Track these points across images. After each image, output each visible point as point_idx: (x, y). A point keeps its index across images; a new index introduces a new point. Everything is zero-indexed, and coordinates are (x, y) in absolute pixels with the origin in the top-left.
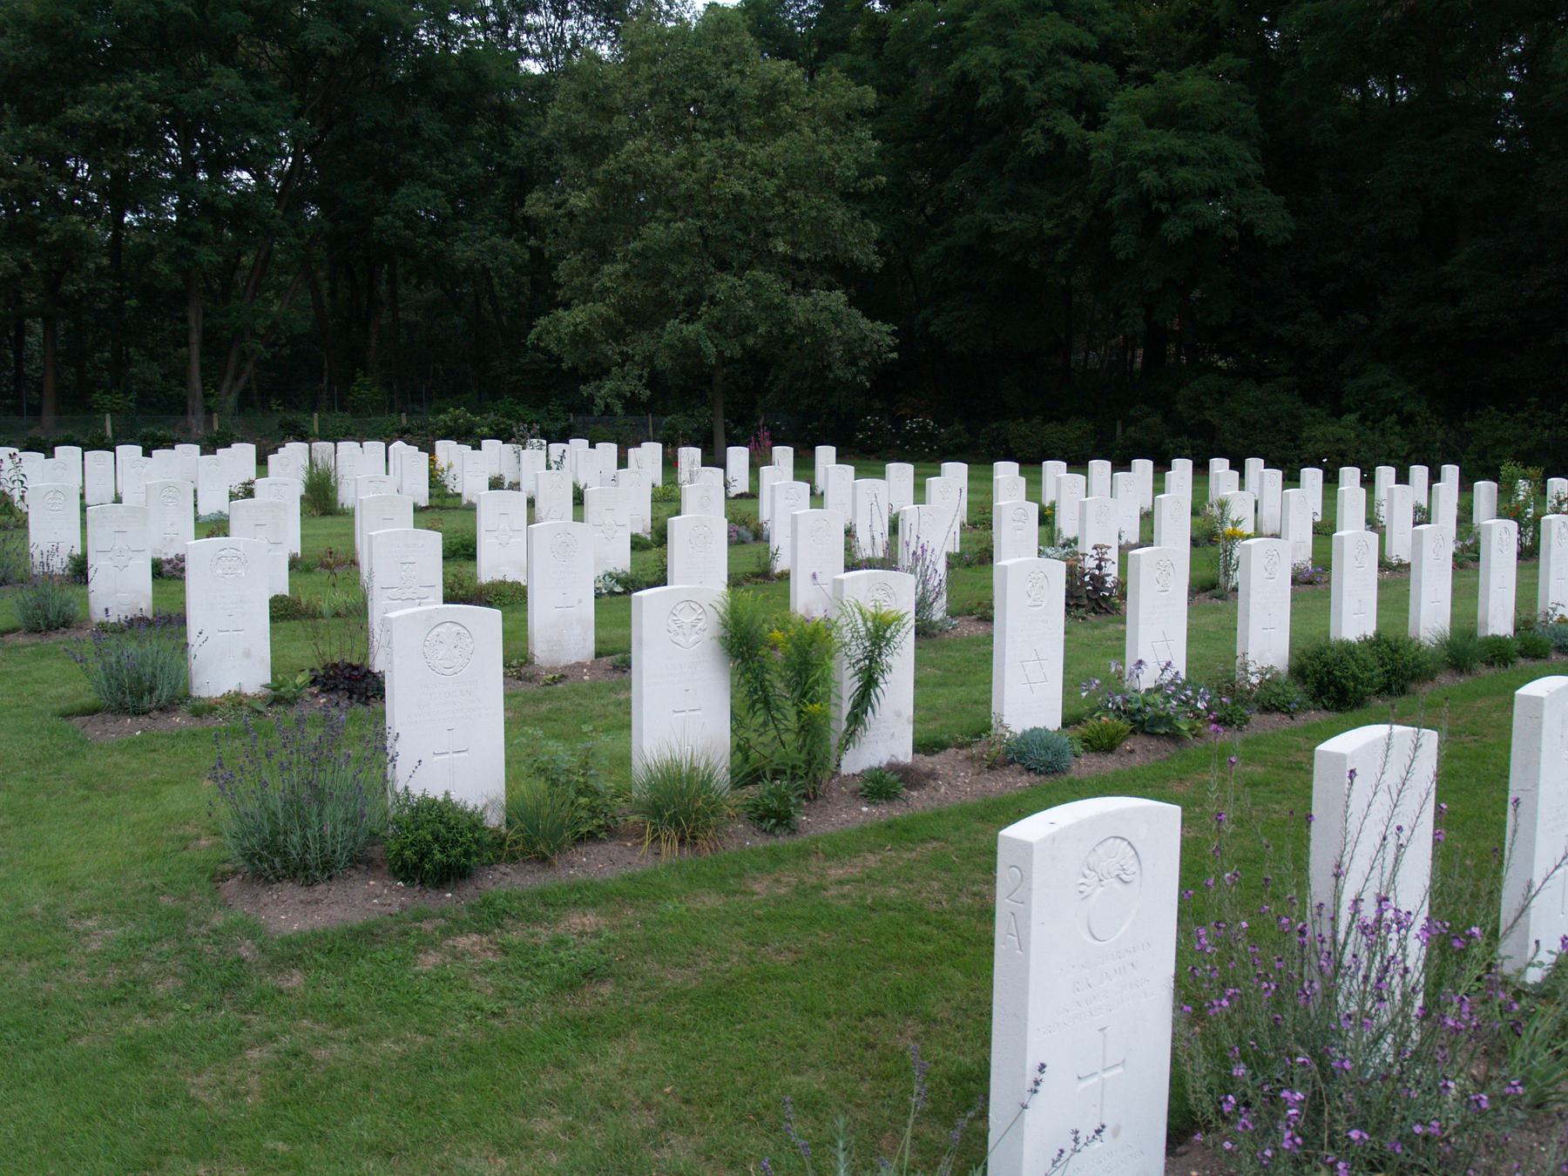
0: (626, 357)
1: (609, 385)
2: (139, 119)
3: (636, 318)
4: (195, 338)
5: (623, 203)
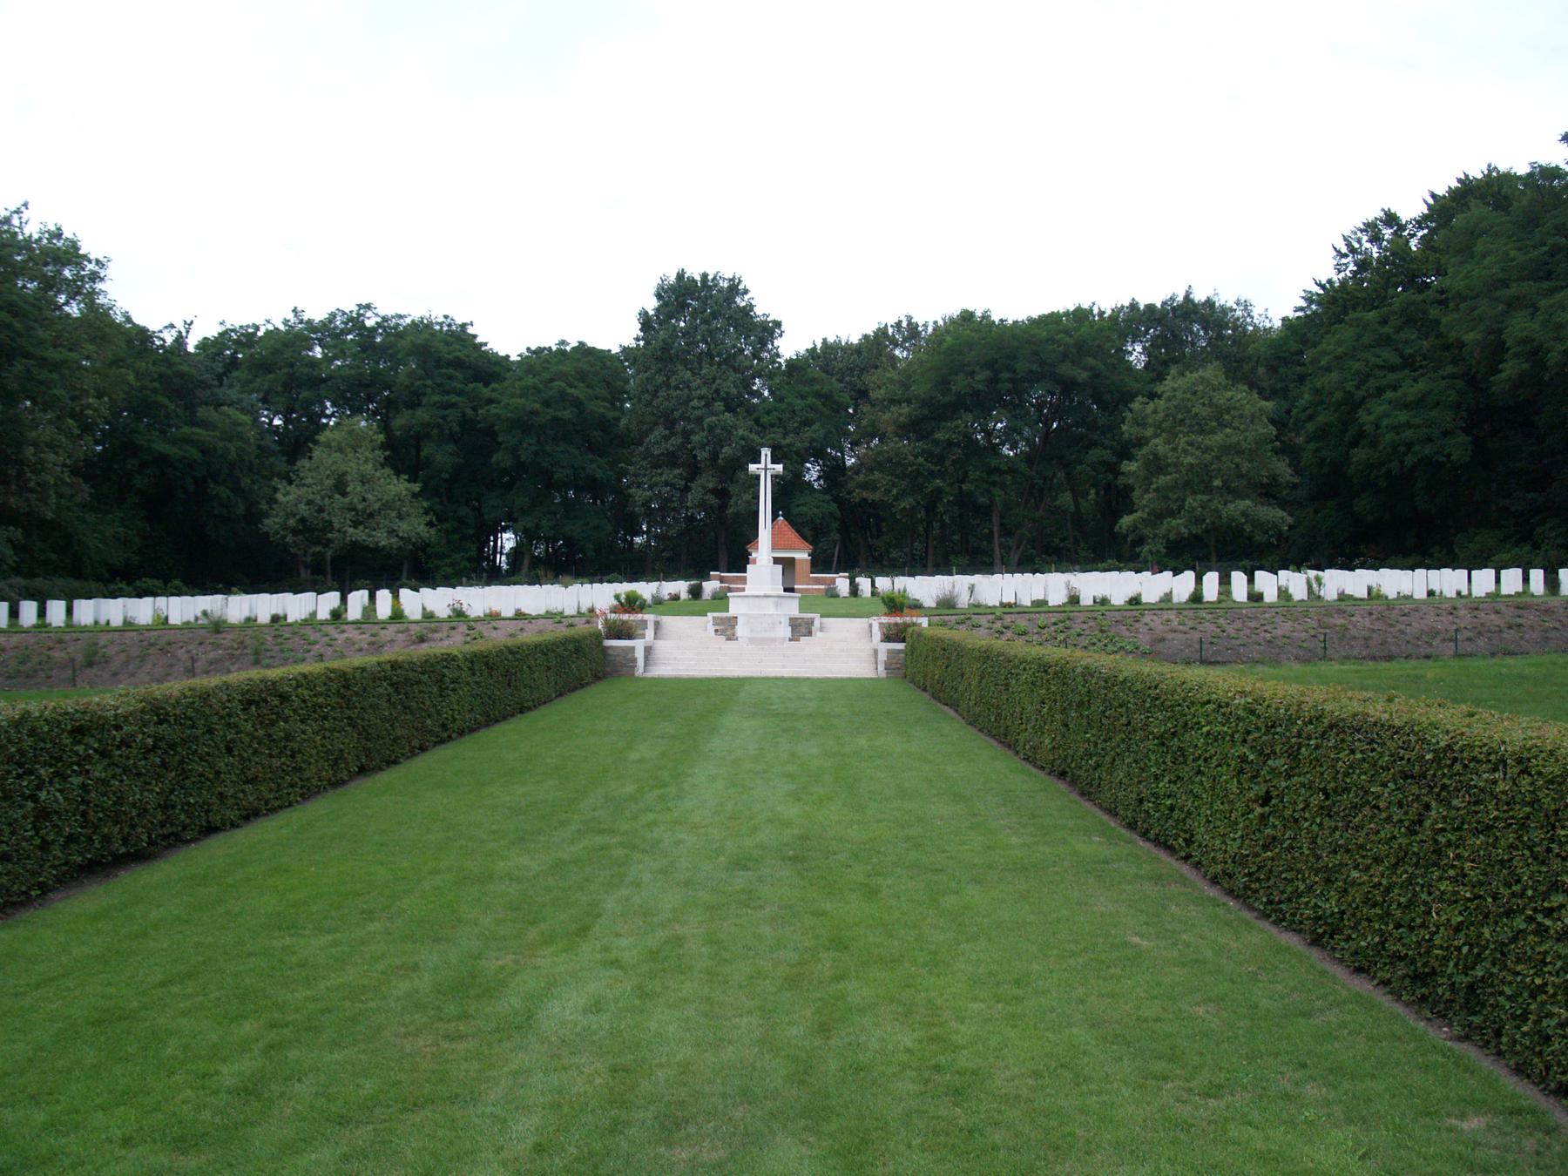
0: (1155, 535)
1: (1146, 548)
2: (965, 436)
3: (1158, 517)
4: (996, 529)
5: (1157, 465)
